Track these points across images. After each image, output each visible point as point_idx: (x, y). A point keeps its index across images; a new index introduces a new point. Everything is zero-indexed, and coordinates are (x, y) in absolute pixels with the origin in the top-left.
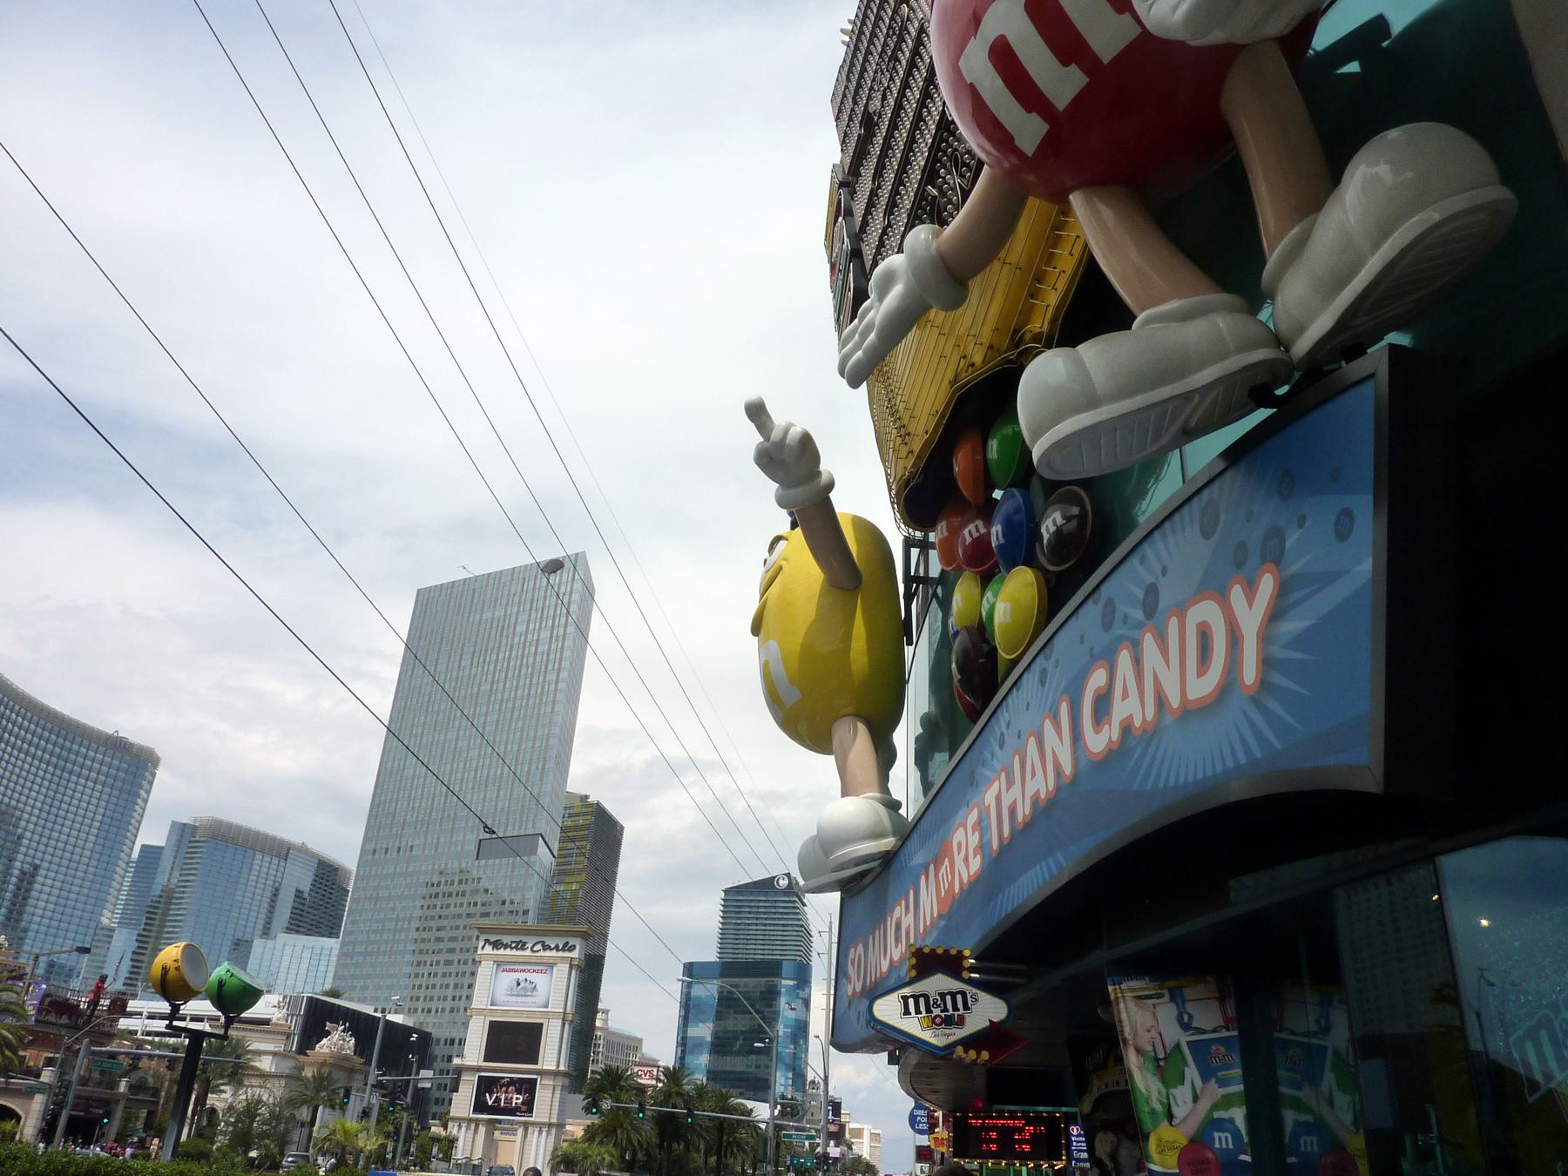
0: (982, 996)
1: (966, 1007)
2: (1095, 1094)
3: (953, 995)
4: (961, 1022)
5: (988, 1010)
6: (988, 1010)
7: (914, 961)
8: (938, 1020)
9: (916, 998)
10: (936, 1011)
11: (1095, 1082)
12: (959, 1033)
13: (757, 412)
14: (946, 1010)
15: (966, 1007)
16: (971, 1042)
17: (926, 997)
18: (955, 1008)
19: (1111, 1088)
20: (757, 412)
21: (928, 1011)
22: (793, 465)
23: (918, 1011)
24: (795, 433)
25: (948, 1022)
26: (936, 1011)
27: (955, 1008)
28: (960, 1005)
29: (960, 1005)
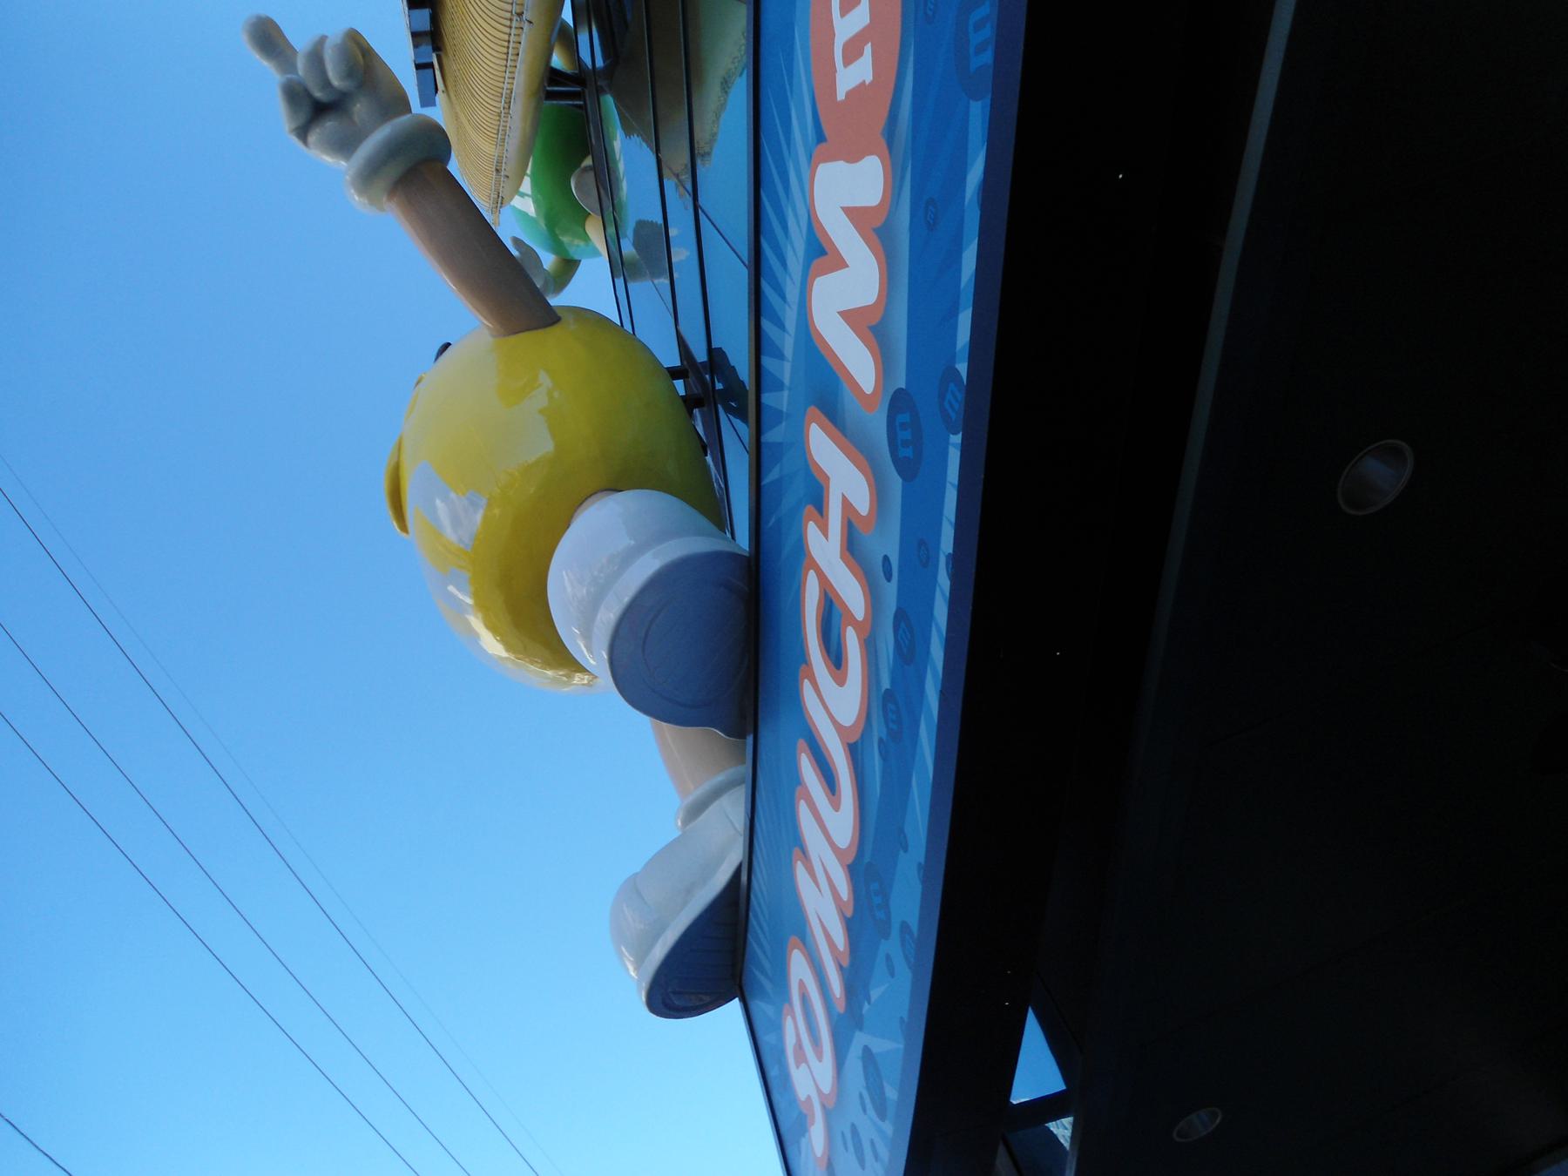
13: (267, 38)
20: (267, 38)
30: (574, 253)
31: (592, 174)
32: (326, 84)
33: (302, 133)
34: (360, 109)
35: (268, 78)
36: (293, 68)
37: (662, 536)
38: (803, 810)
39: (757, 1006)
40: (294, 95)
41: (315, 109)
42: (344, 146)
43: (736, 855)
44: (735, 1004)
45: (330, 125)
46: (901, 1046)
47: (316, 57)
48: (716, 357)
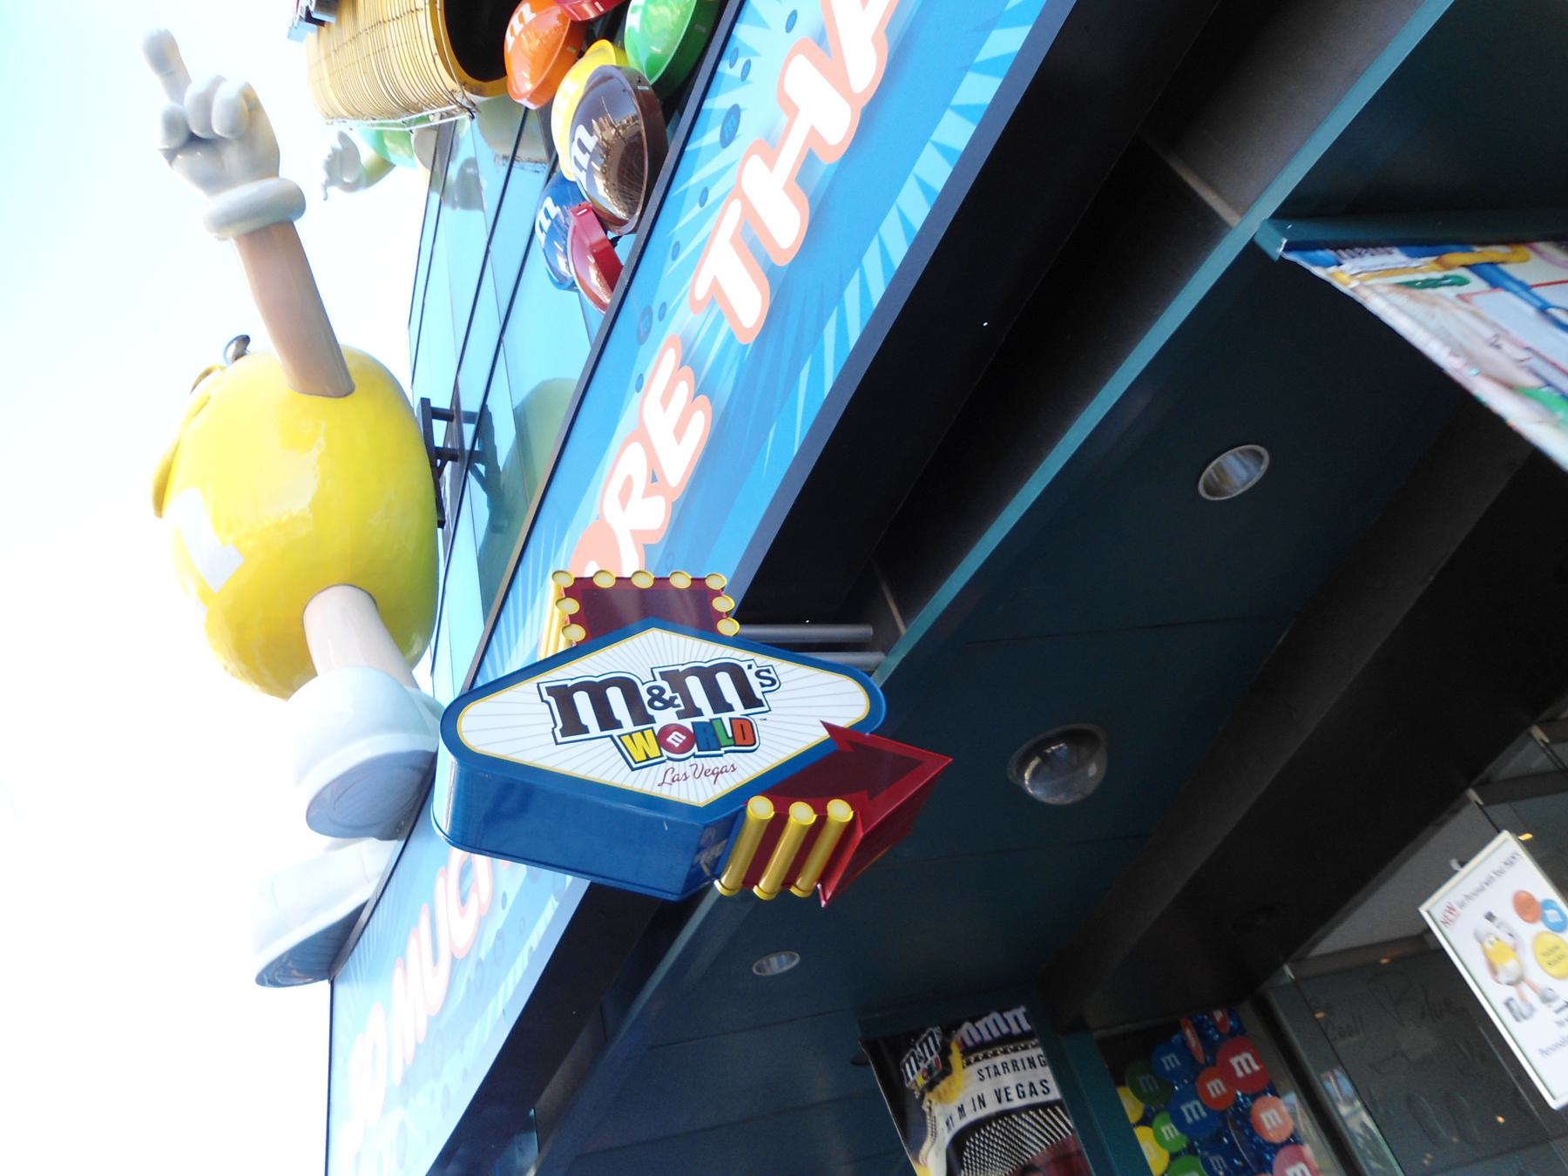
0: (785, 669)
1: (750, 700)
2: (945, 1137)
3: (707, 676)
4: (745, 736)
5: (813, 703)
6: (813, 703)
7: (573, 606)
8: (675, 739)
9: (597, 692)
10: (665, 717)
11: (937, 1110)
12: (748, 766)
13: (164, 56)
14: (692, 710)
15: (750, 700)
16: (787, 784)
17: (629, 688)
18: (719, 704)
19: (971, 1116)
20: (164, 56)
21: (641, 717)
22: (218, 81)
23: (607, 720)
24: (227, 93)
25: (704, 739)
26: (665, 717)
27: (719, 704)
28: (730, 693)
29: (730, 693)
30: (393, 159)
31: (434, 134)
32: (208, 127)
33: (171, 155)
34: (232, 157)
35: (153, 101)
36: (180, 100)
37: (388, 727)
38: (413, 942)
39: (339, 989)
40: (173, 124)
41: (190, 140)
42: (212, 182)
43: (366, 892)
44: (325, 984)
45: (198, 156)
46: (675, 18)
47: (205, 102)
48: (483, 419)
